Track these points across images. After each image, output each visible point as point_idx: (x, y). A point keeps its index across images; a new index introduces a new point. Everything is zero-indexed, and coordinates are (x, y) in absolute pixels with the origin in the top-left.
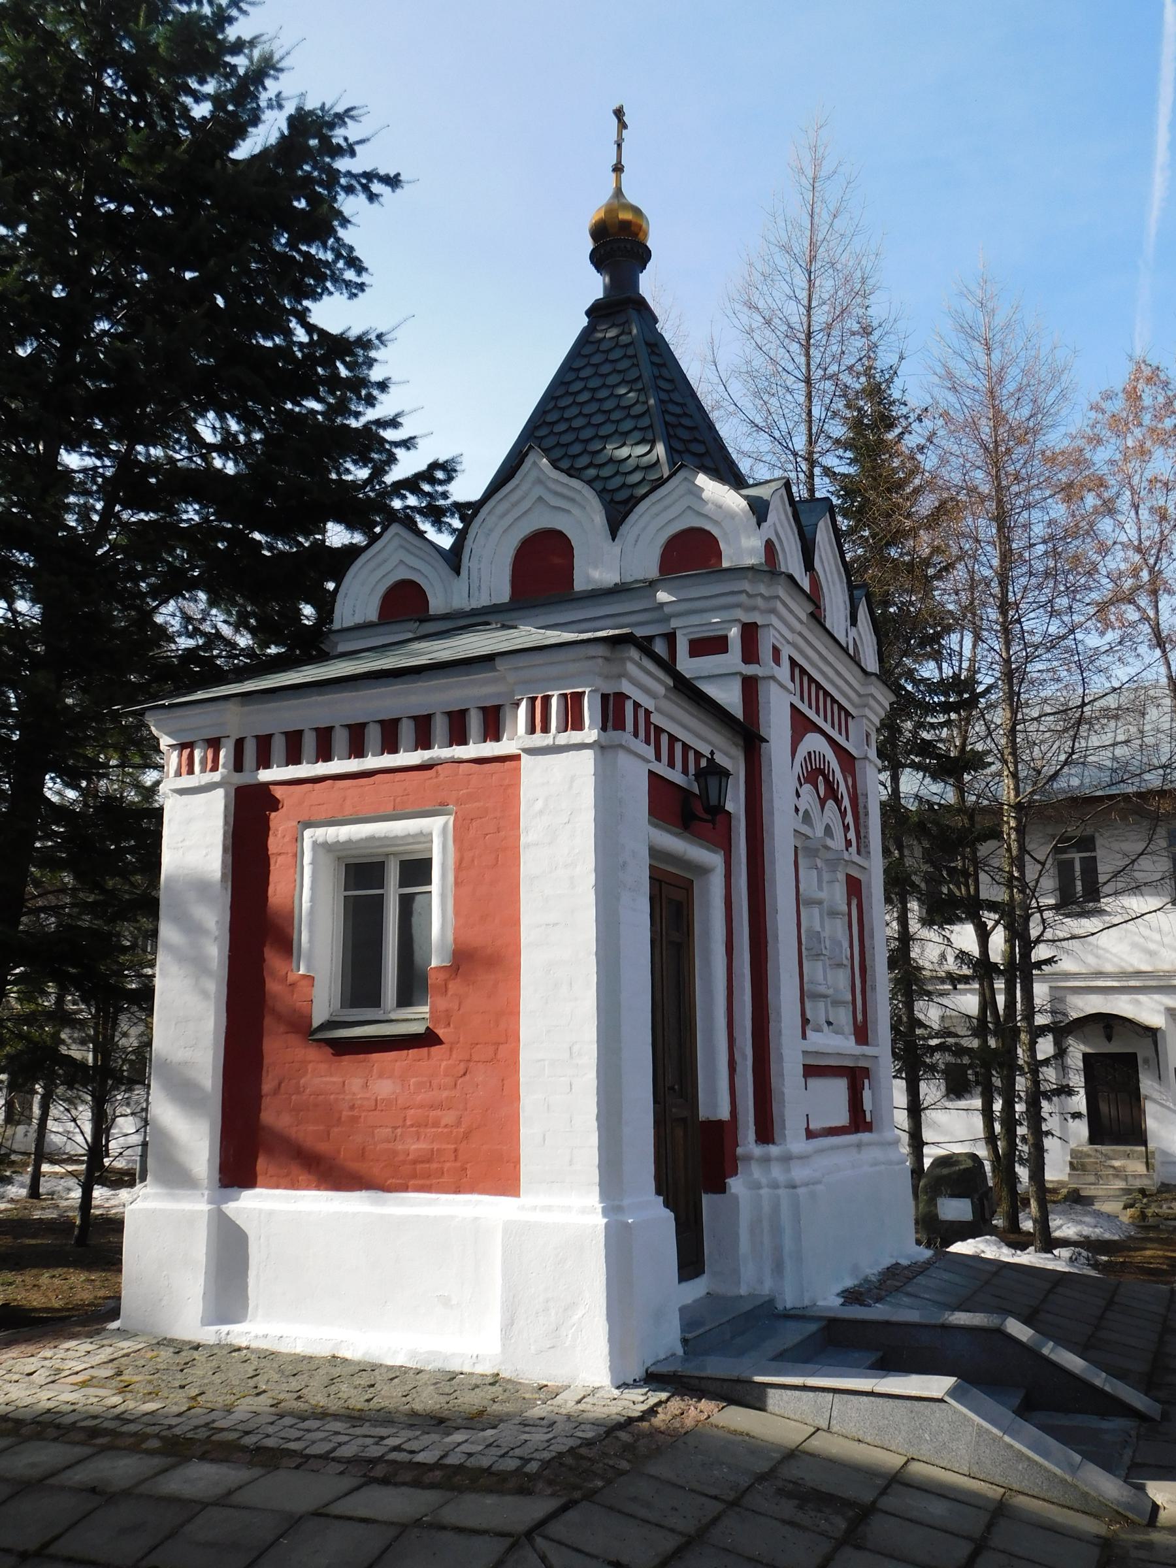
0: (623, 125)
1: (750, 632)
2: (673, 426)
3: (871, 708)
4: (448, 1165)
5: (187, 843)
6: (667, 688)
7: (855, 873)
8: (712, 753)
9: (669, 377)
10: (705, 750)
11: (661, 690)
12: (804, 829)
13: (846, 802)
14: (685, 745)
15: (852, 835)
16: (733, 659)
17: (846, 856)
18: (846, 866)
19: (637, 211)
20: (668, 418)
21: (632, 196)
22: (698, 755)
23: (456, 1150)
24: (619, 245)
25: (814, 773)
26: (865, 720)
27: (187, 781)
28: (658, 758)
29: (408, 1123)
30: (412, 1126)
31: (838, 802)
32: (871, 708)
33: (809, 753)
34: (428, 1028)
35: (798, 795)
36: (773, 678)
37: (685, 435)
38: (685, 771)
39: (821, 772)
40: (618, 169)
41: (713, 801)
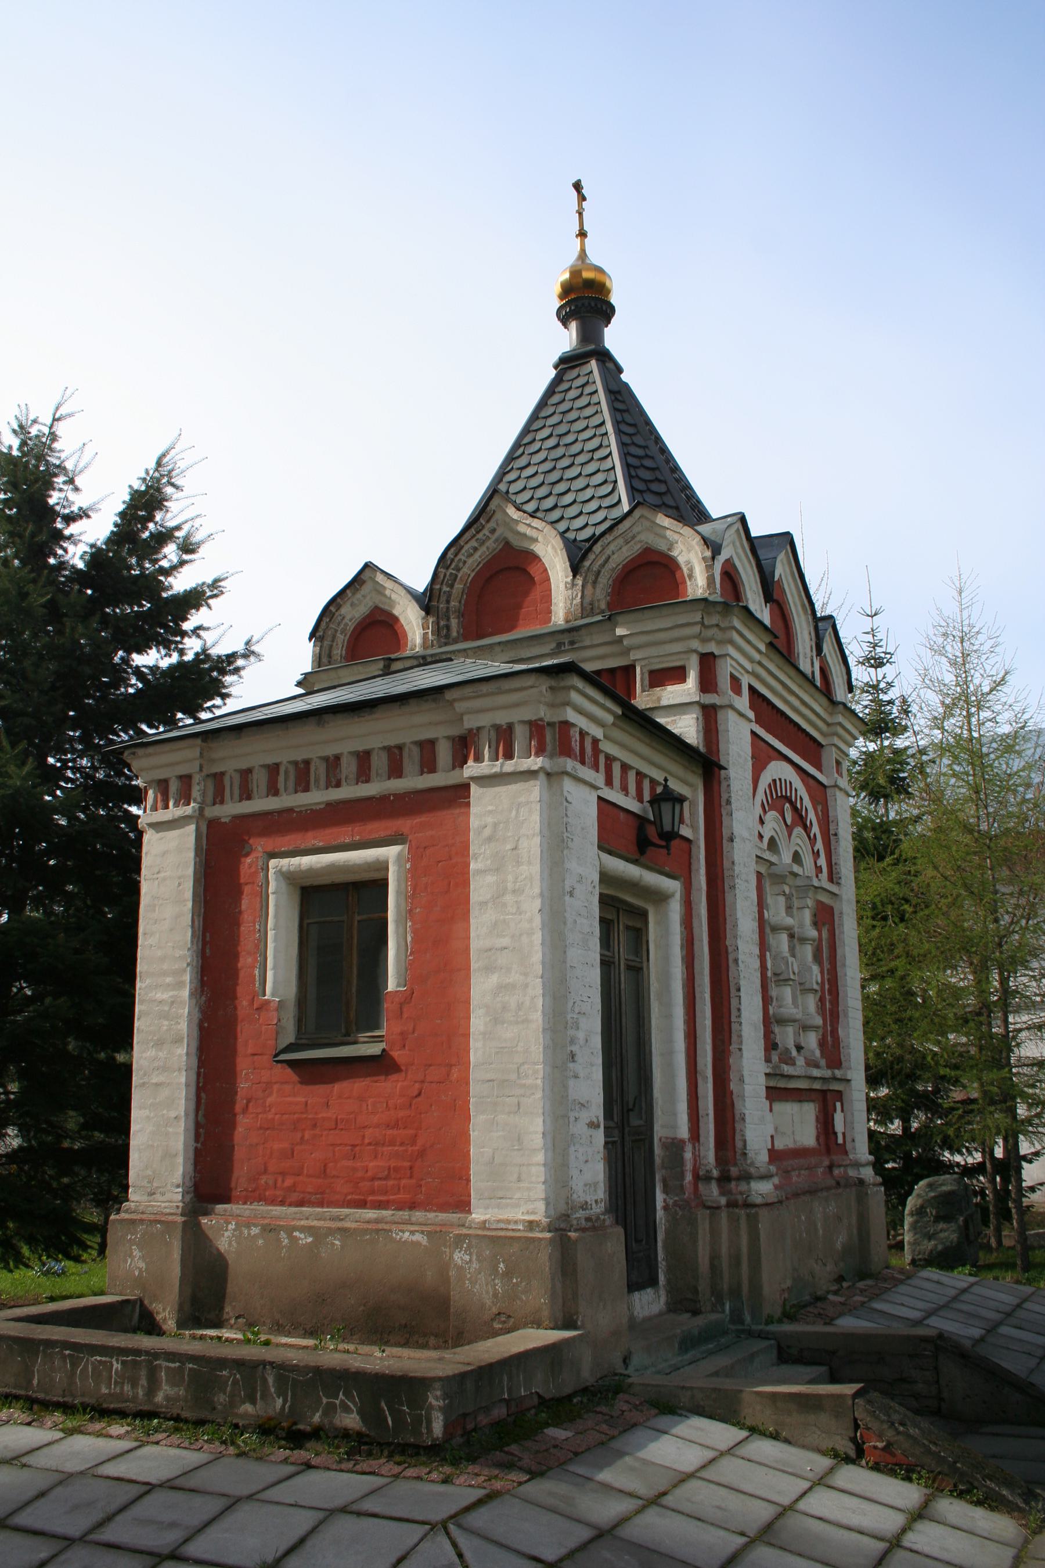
0: (582, 198)
1: (708, 663)
2: (635, 467)
3: (840, 737)
4: (403, 1182)
5: (162, 875)
6: (616, 716)
7: (824, 898)
8: (666, 780)
9: (632, 422)
10: (659, 776)
11: (610, 719)
12: (767, 855)
13: (815, 829)
14: (639, 774)
15: (822, 861)
16: (688, 689)
17: (816, 883)
18: (816, 893)
19: (599, 270)
20: (630, 460)
21: (595, 258)
22: (653, 782)
23: (411, 1168)
24: (586, 302)
25: (779, 799)
26: (834, 749)
27: (162, 815)
28: (609, 782)
29: (367, 1141)
30: (370, 1144)
31: (807, 829)
32: (840, 737)
33: (774, 781)
34: (384, 1050)
35: (762, 822)
36: (731, 707)
37: (647, 475)
38: (640, 798)
39: (788, 799)
40: (582, 234)
41: (667, 827)
